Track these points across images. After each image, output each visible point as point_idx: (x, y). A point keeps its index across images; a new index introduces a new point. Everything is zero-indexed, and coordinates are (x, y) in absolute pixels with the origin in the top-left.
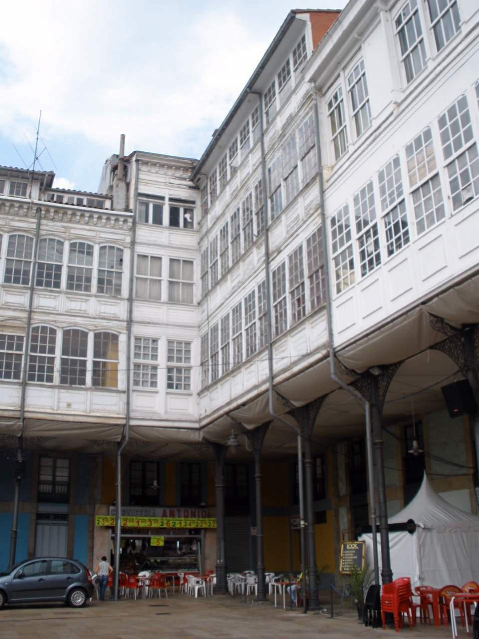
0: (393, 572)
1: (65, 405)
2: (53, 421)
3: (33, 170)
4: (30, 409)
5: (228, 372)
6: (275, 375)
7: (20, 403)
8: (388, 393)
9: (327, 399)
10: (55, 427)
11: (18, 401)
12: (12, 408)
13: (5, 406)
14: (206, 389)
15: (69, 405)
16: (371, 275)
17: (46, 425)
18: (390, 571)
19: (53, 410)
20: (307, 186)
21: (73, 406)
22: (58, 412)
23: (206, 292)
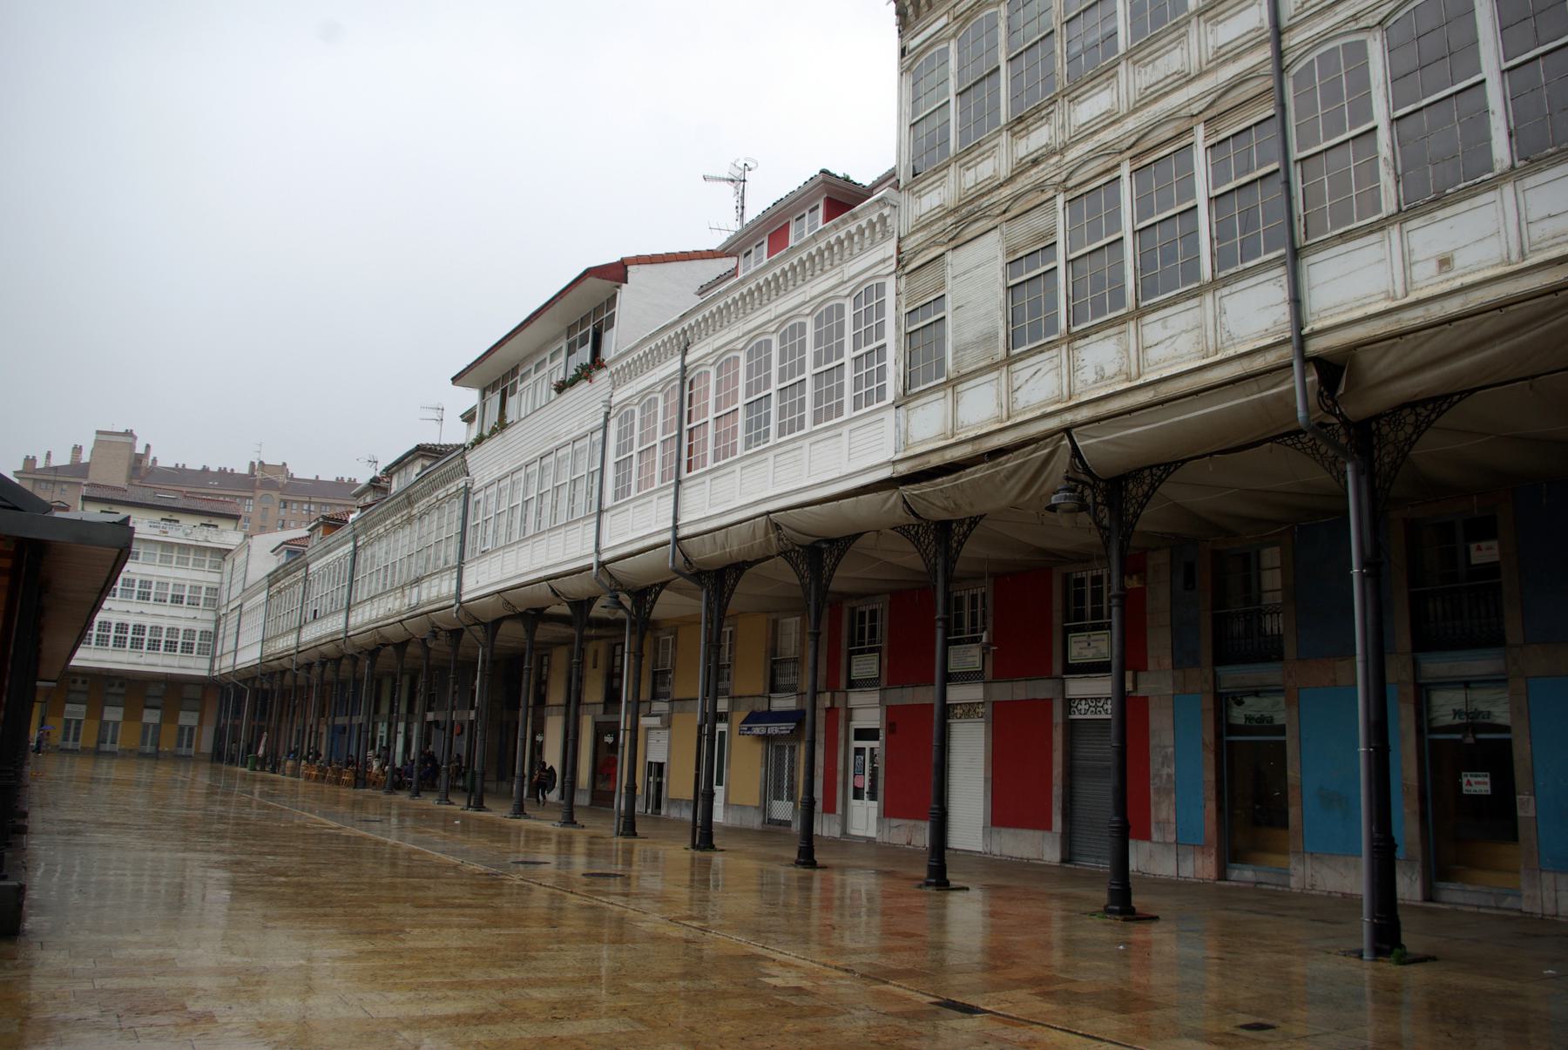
0: (1397, 841)
1: (1433, 266)
2: (1401, 335)
3: (584, 854)
4: (1318, 326)
5: (1022, 231)
6: (1269, 42)
7: (1287, 318)
8: (734, 595)
9: (860, 540)
10: (1418, 355)
11: (1283, 313)
12: (1269, 341)
13: (1252, 340)
14: (905, 450)
15: (1445, 263)
16: (668, 778)
17: (1426, 347)
18: (1392, 839)
19: (1394, 299)
20: (287, 632)
21: (1459, 262)
22: (1412, 298)
23: (415, 590)
